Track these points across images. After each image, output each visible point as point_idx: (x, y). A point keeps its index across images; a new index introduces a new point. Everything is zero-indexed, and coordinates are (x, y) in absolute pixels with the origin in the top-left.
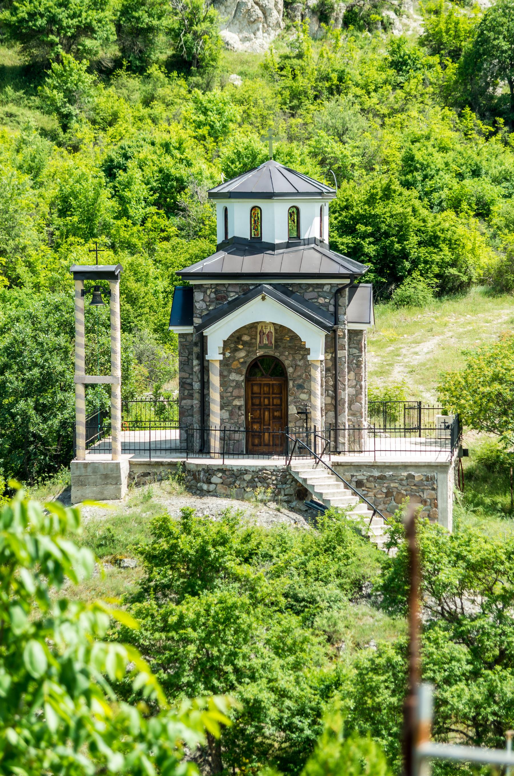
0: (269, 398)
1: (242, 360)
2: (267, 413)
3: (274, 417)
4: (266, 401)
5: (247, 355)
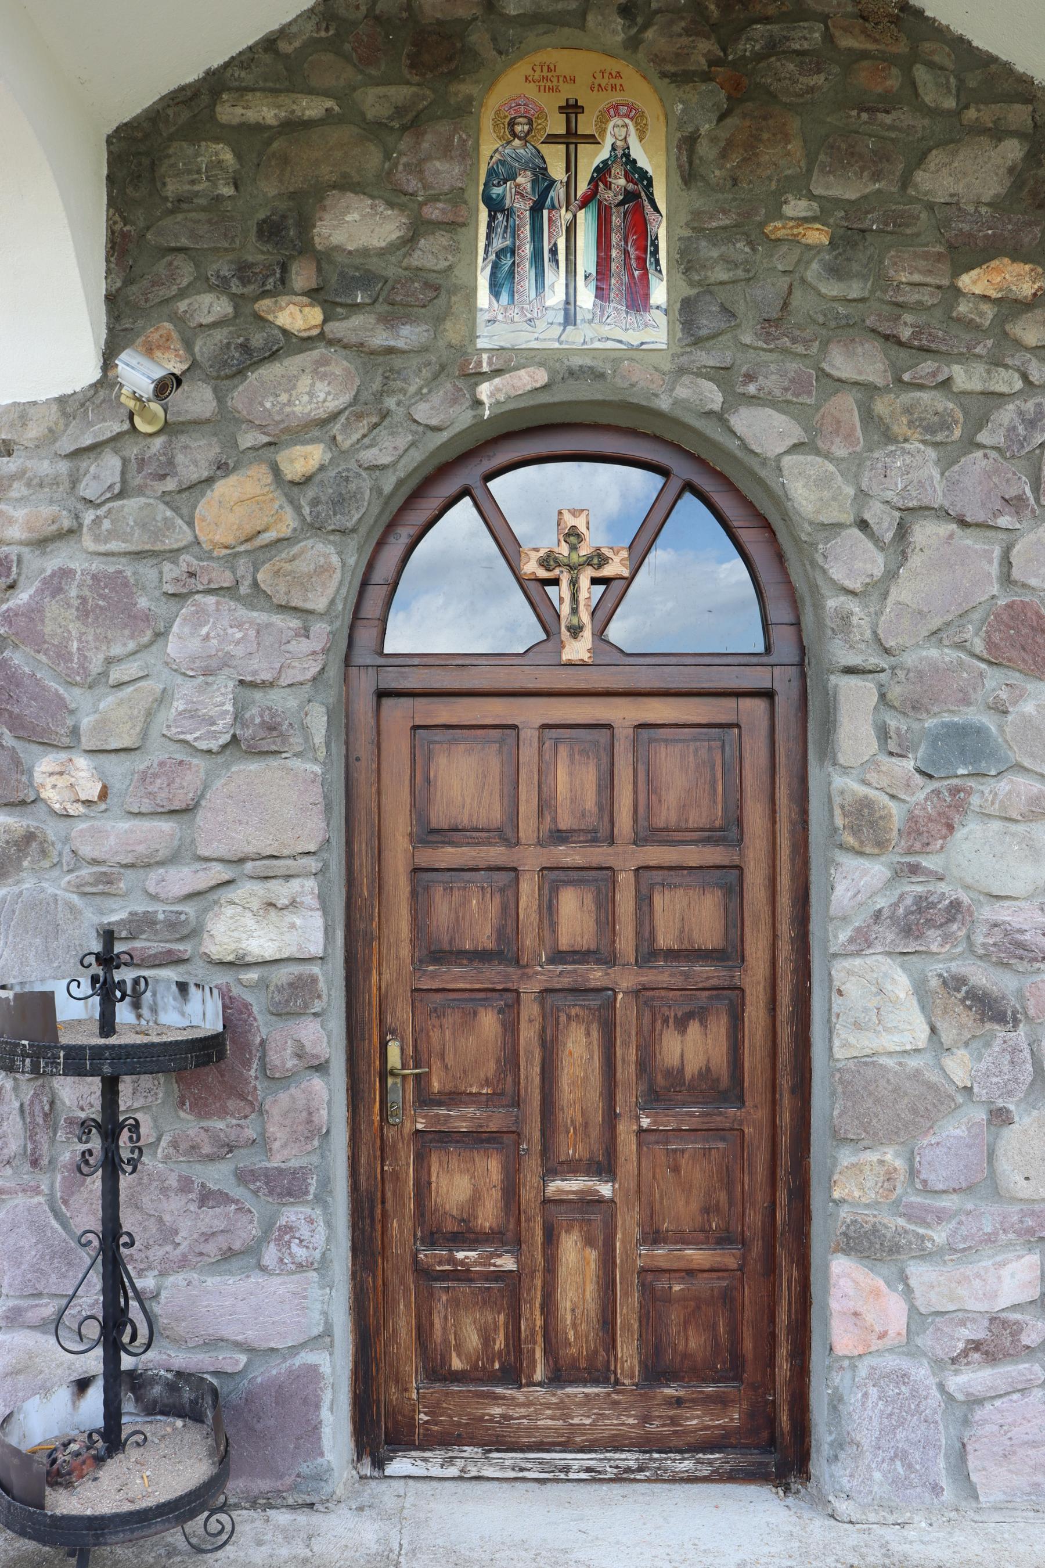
0: (600, 880)
1: (303, 459)
2: (579, 1049)
3: (661, 1089)
4: (574, 916)
5: (370, 410)
